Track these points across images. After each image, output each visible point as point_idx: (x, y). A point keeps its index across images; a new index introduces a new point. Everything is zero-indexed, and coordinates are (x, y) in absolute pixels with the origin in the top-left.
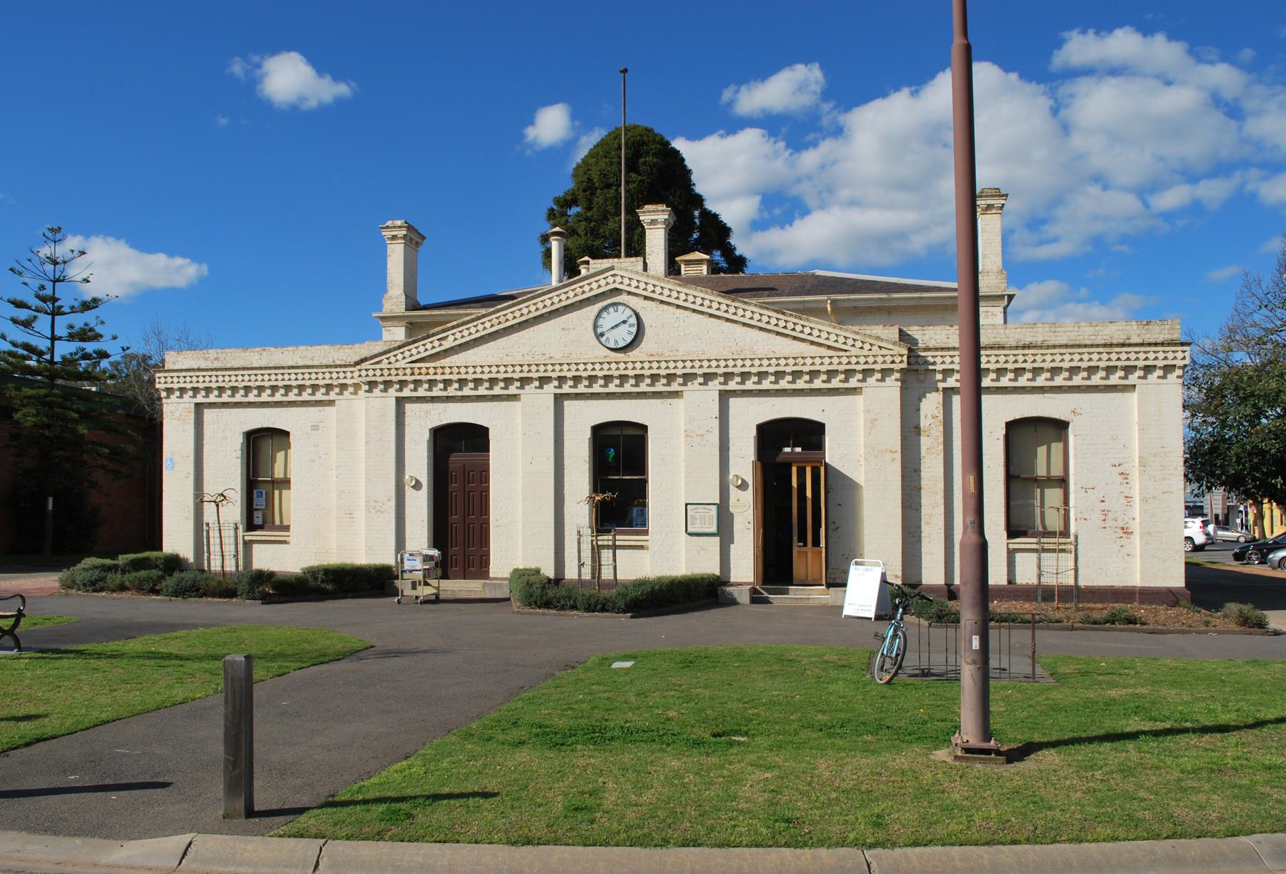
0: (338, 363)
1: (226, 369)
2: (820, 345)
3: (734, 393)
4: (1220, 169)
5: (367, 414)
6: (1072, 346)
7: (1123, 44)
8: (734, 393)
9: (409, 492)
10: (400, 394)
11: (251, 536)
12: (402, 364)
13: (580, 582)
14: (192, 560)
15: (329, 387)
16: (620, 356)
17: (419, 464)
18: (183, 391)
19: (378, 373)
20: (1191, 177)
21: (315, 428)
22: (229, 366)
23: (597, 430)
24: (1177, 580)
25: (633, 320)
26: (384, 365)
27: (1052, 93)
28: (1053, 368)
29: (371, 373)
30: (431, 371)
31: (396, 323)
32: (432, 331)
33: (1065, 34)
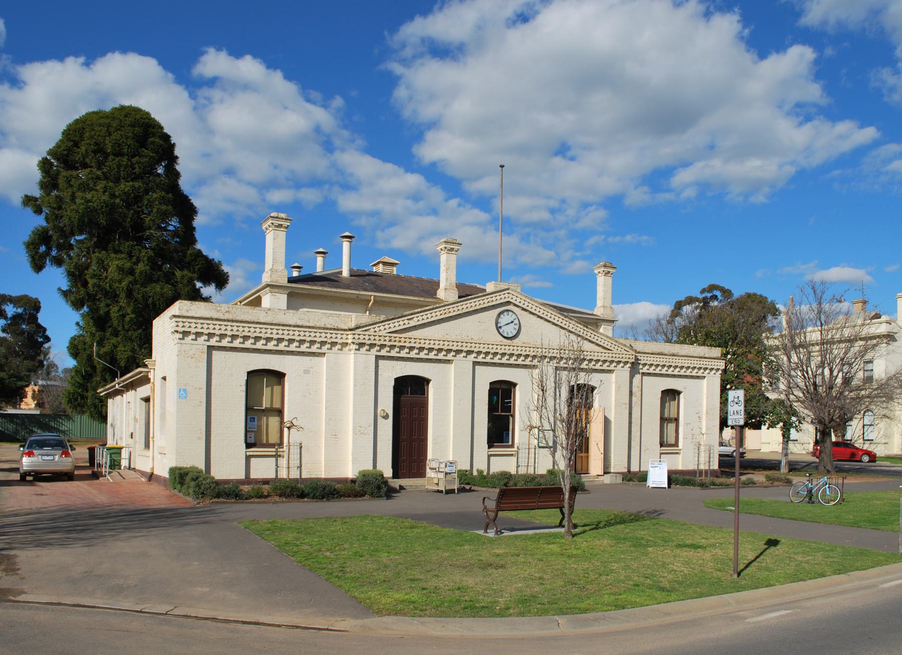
0: (329, 326)
2: (600, 346)
3: (479, 363)
4: (315, 183)
5: (352, 365)
7: (249, 68)
8: (479, 363)
9: (380, 420)
10: (379, 354)
11: (253, 451)
12: (383, 333)
14: (204, 469)
15: (323, 343)
16: (509, 342)
17: (387, 403)
18: (198, 334)
19: (367, 337)
20: (297, 184)
21: (306, 372)
22: (238, 318)
23: (397, 380)
25: (516, 321)
26: (372, 332)
27: (193, 96)
29: (362, 337)
30: (403, 340)
31: (281, 291)
32: (405, 313)
33: (204, 49)
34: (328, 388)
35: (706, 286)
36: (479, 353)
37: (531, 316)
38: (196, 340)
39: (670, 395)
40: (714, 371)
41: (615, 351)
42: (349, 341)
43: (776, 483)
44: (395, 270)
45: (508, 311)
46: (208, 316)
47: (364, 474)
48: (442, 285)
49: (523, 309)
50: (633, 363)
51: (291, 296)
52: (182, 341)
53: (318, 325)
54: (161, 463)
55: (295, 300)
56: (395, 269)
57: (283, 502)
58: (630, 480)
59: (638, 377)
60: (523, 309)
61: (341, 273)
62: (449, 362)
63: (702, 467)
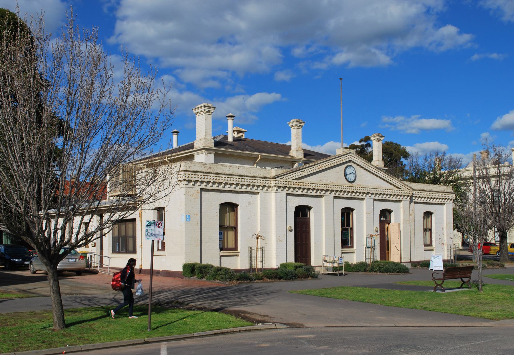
0: (261, 176)
1: (214, 173)
6: (233, 175)
9: (288, 232)
11: (224, 252)
12: (290, 180)
13: (375, 262)
18: (196, 182)
21: (249, 204)
22: (215, 172)
24: (180, 269)
26: (284, 179)
28: (202, 181)
31: (211, 152)
34: (261, 214)
35: (363, 137)
36: (337, 191)
37: (361, 169)
38: (194, 185)
39: (428, 214)
40: (406, 197)
41: (403, 189)
42: (272, 185)
43: (496, 267)
44: (244, 136)
45: (350, 166)
46: (200, 170)
47: (282, 265)
48: (293, 148)
49: (358, 165)
50: (411, 196)
51: (216, 155)
52: (187, 186)
53: (255, 175)
54: (172, 261)
55: (219, 157)
56: (244, 135)
57: (272, 282)
58: (415, 266)
59: (412, 204)
60: (358, 165)
61: (226, 137)
62: (321, 197)
63: (254, 267)
